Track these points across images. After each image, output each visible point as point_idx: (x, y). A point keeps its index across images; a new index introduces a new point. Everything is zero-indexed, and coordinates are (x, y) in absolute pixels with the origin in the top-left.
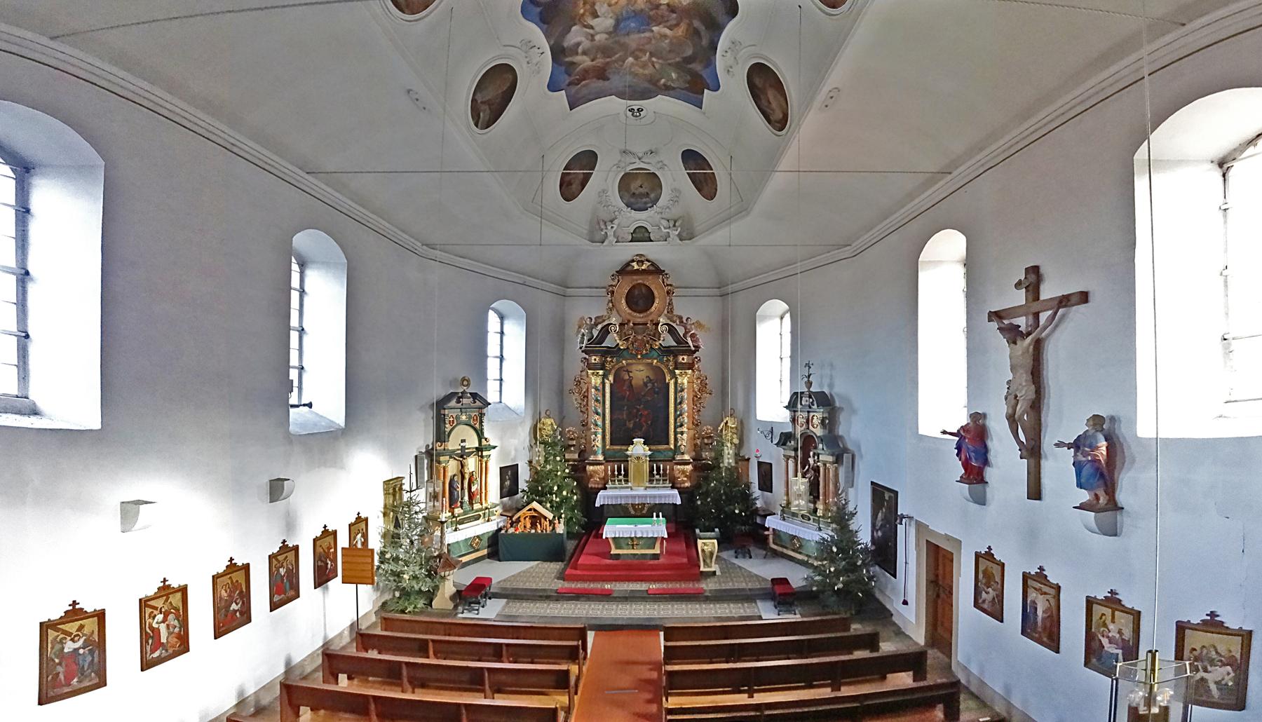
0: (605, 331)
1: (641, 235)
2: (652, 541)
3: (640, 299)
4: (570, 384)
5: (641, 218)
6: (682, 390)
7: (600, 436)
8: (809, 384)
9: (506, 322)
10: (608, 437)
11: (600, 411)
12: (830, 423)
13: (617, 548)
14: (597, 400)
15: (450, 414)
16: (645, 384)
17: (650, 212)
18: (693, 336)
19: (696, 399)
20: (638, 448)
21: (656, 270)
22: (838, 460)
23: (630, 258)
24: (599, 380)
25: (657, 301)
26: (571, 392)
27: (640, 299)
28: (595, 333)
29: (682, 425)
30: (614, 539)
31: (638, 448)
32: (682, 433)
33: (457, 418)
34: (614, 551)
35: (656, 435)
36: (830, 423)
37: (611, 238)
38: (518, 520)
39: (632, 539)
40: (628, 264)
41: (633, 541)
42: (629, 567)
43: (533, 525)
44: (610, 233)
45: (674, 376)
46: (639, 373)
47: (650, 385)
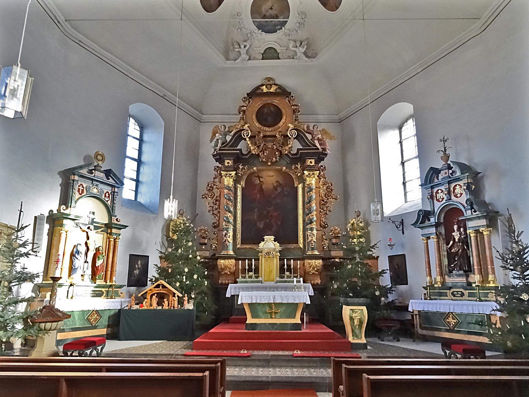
0: (238, 137)
1: (270, 54)
2: (291, 308)
3: (269, 116)
4: (202, 189)
5: (270, 40)
6: (311, 190)
7: (231, 233)
8: (447, 157)
9: (145, 131)
10: (239, 236)
11: (232, 209)
12: (475, 188)
13: (253, 317)
14: (229, 200)
15: (81, 183)
16: (275, 188)
17: (280, 33)
18: (319, 139)
19: (322, 204)
20: (269, 244)
21: (283, 92)
22: (492, 223)
23: (260, 83)
24: (231, 183)
25: (284, 117)
26: (204, 197)
27: (269, 116)
28: (228, 138)
29: (311, 222)
30: (250, 305)
31: (269, 244)
32: (312, 229)
33: (88, 189)
34: (250, 320)
35: (286, 235)
36: (475, 188)
37: (244, 56)
38: (144, 297)
39: (269, 304)
40: (258, 88)
41: (271, 308)
42: (268, 336)
43: (159, 304)
44: (243, 51)
45: (302, 180)
46: (270, 178)
47: (279, 189)
